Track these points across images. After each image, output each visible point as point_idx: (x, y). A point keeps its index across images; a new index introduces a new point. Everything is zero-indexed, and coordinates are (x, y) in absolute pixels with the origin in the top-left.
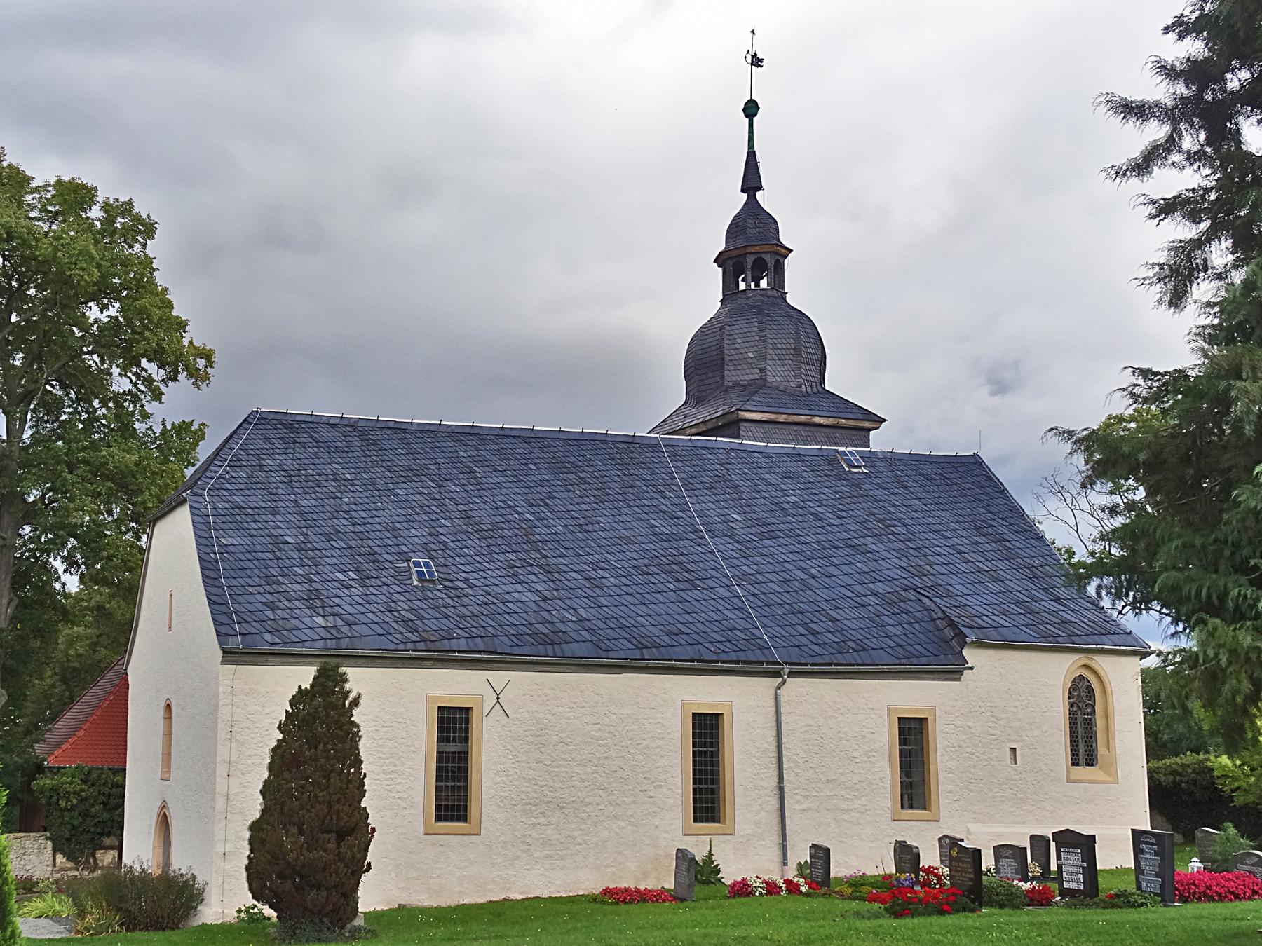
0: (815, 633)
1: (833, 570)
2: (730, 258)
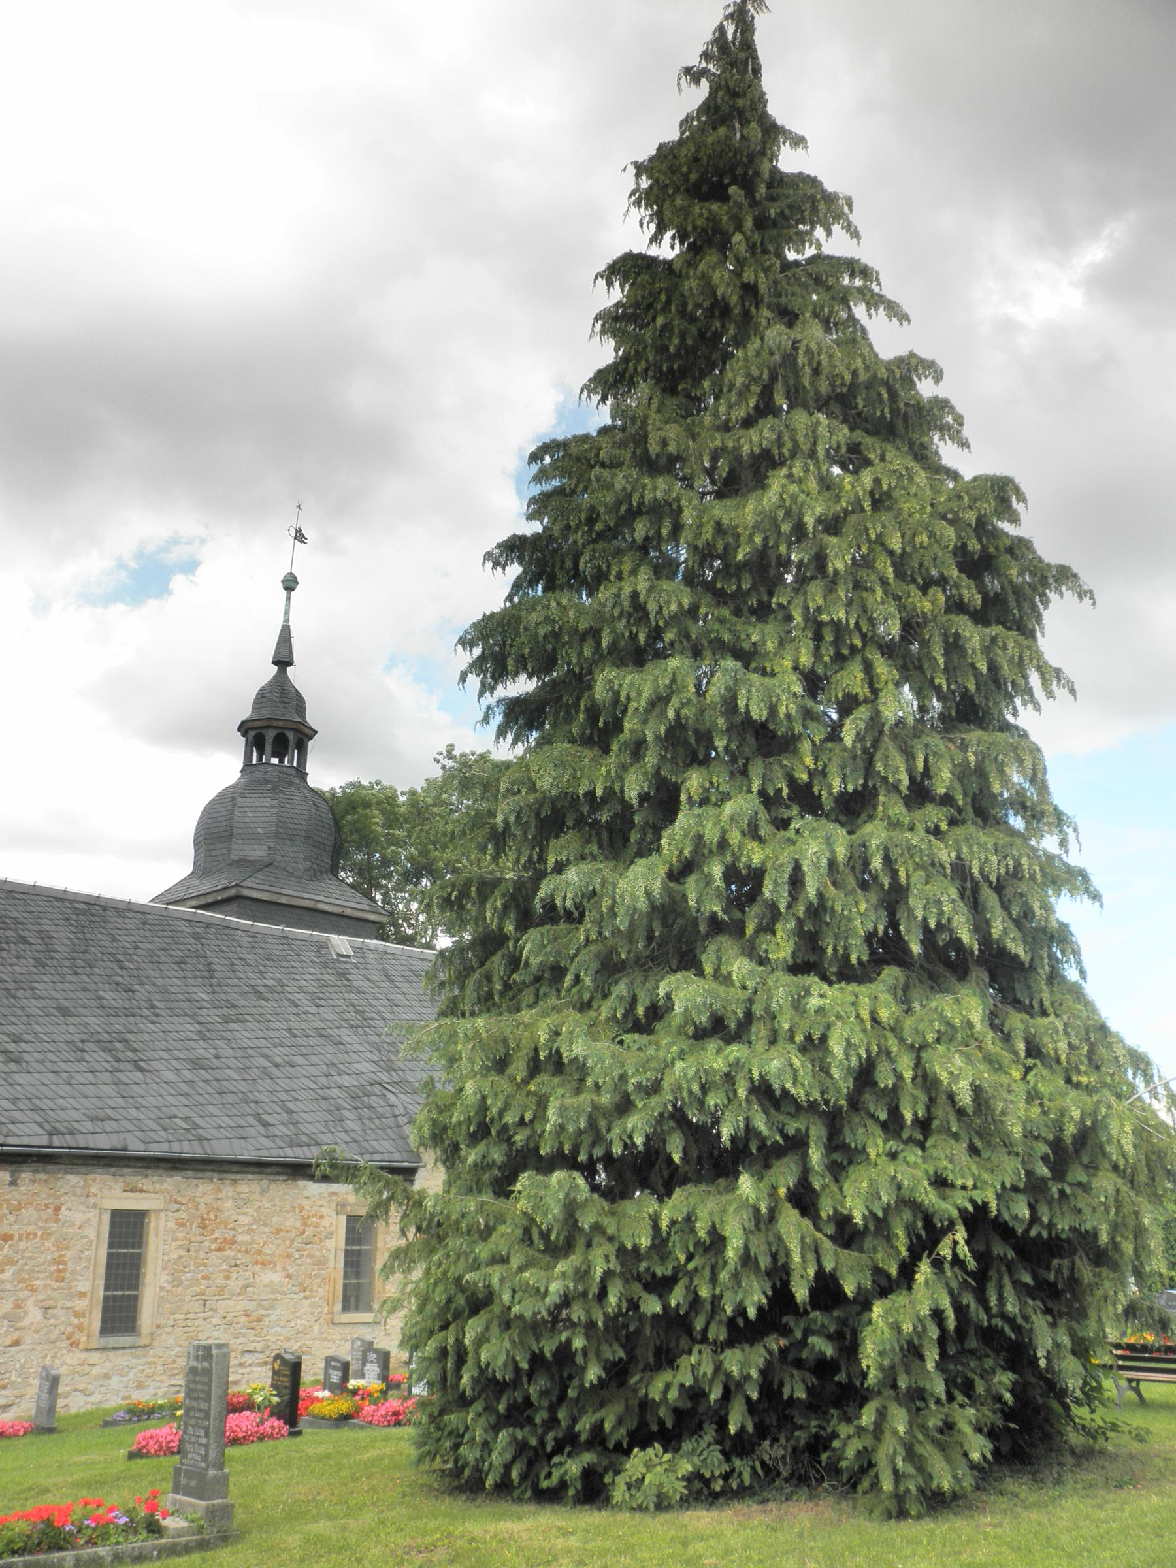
0: (266, 1125)
1: (299, 1060)
2: (253, 729)
